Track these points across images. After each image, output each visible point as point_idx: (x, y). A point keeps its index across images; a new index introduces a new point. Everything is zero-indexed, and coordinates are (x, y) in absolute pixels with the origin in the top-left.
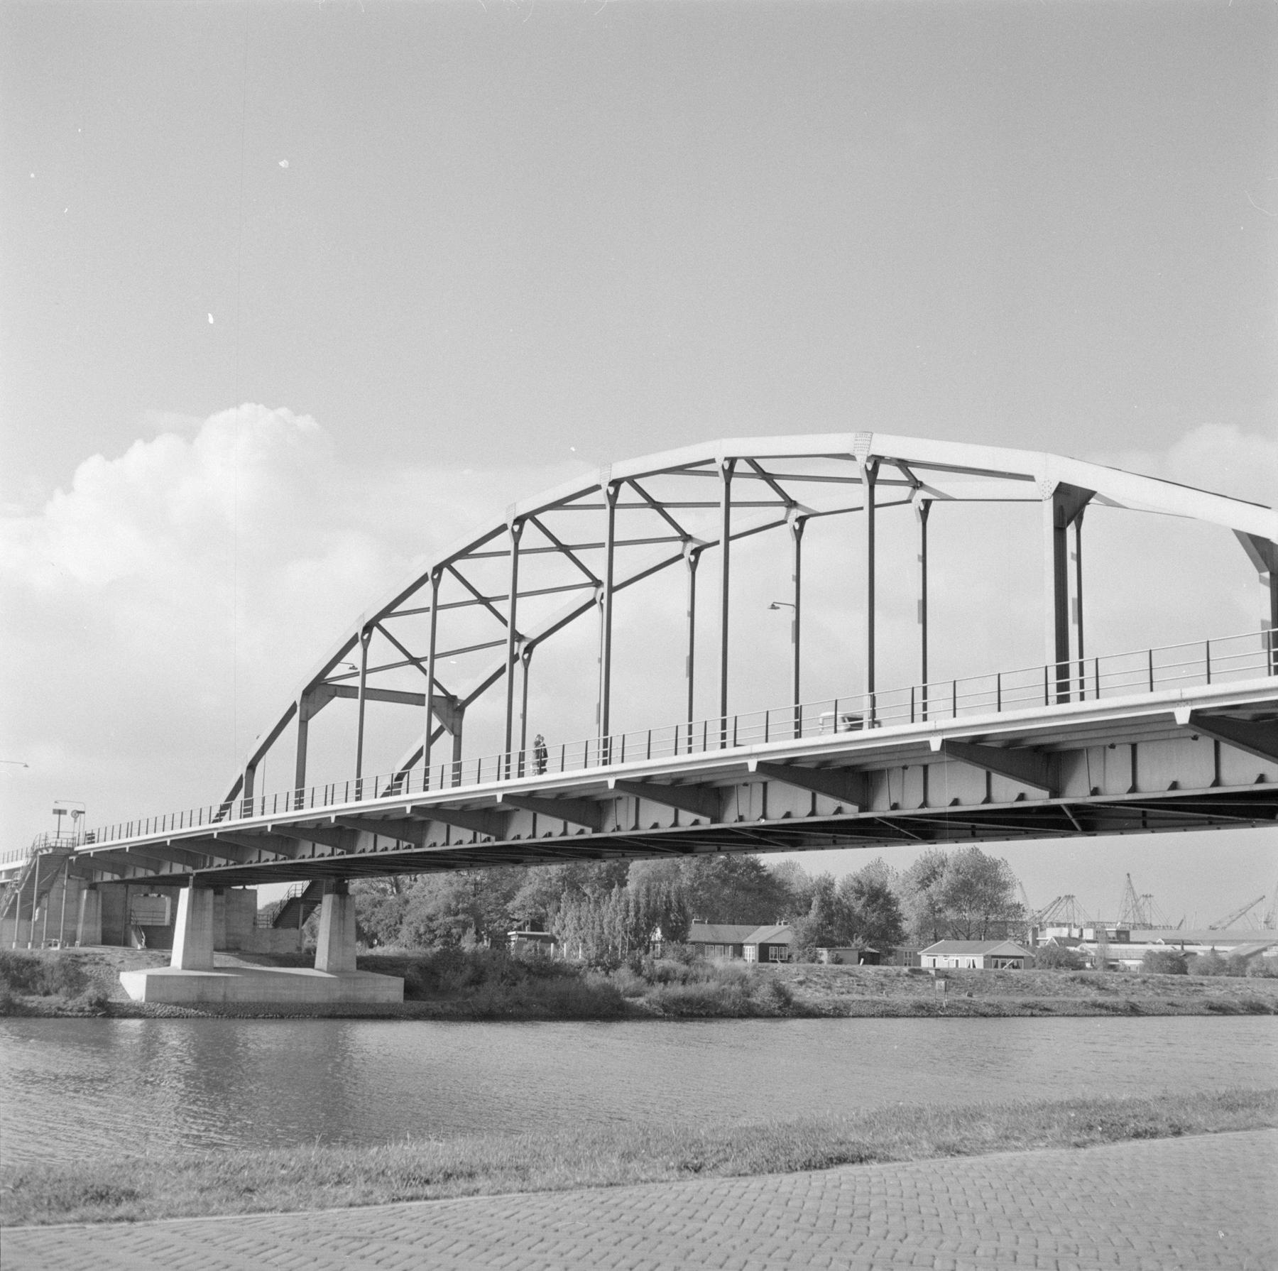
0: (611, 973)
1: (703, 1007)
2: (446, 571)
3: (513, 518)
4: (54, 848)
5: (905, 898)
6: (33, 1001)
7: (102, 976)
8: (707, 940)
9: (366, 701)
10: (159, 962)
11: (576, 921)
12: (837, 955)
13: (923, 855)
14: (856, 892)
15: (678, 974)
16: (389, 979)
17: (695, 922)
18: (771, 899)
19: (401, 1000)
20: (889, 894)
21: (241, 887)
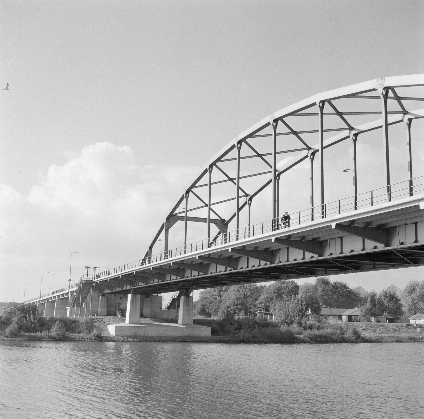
0: (290, 326)
1: (326, 339)
2: (214, 166)
3: (237, 141)
4: (86, 280)
5: (403, 299)
6: (73, 335)
7: (101, 327)
8: (328, 314)
9: (188, 222)
10: (122, 321)
11: (279, 308)
12: (378, 319)
13: (410, 282)
14: (385, 296)
15: (316, 326)
16: (205, 328)
17: (324, 307)
18: (353, 299)
19: (210, 336)
20: (397, 297)
21: (156, 295)
